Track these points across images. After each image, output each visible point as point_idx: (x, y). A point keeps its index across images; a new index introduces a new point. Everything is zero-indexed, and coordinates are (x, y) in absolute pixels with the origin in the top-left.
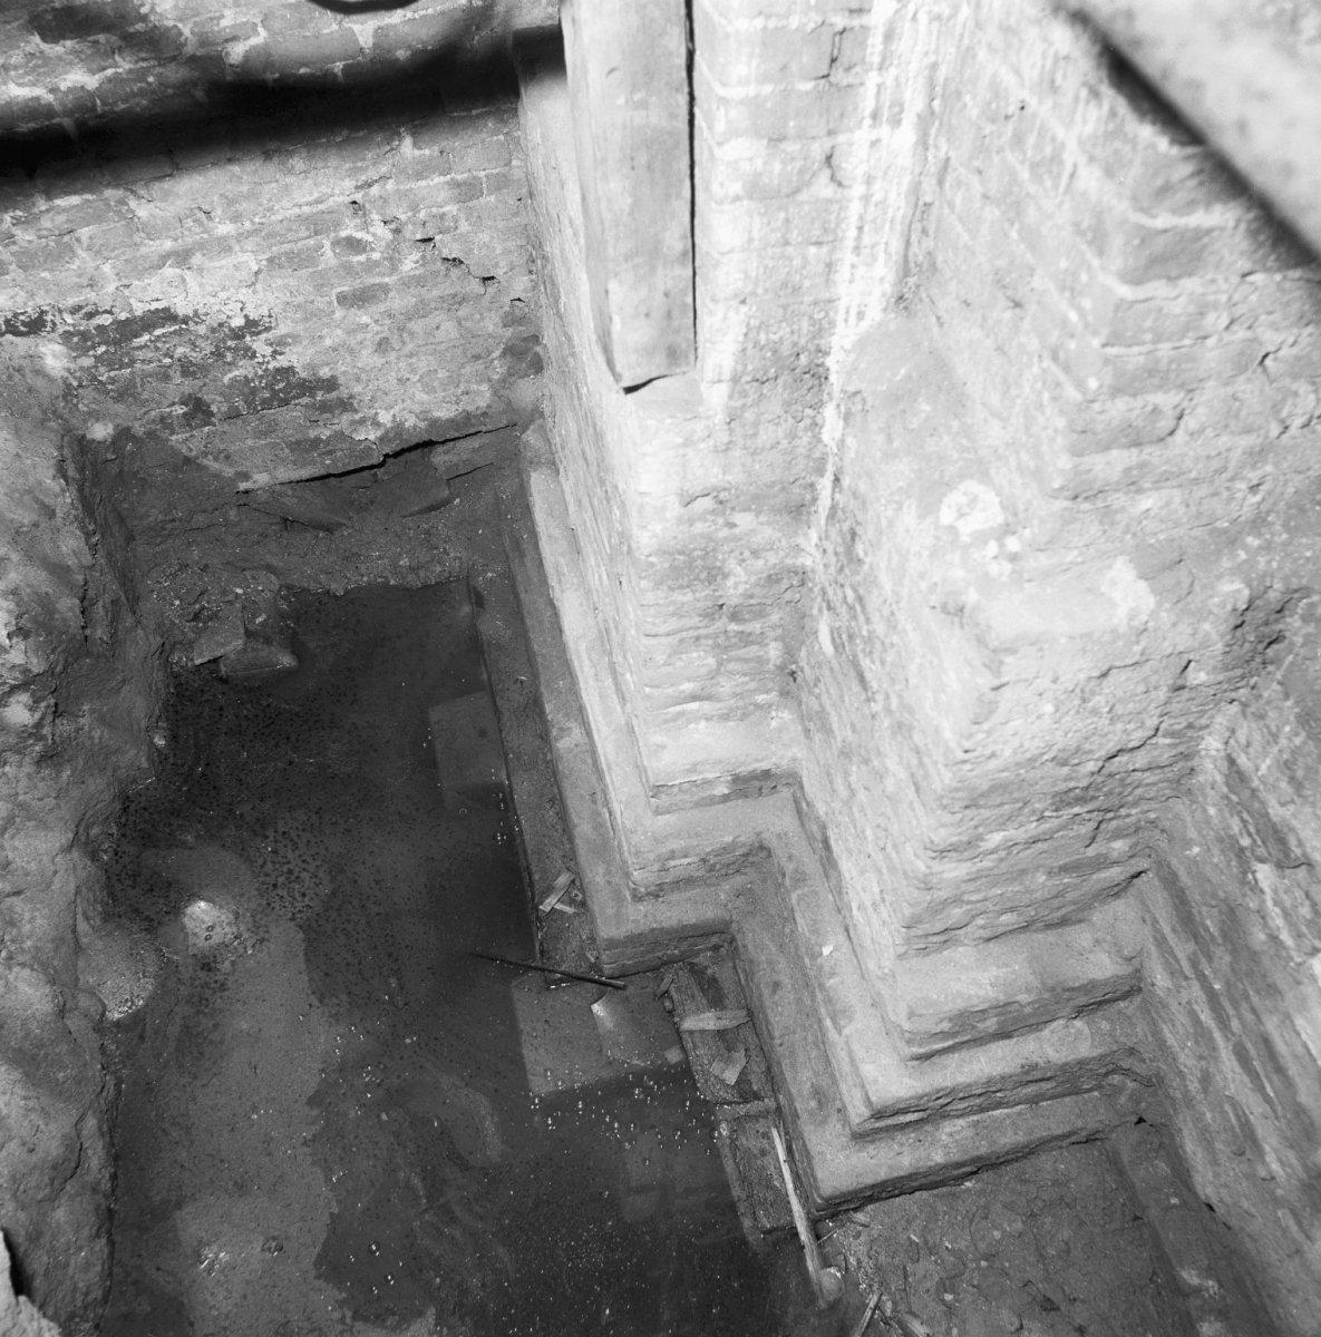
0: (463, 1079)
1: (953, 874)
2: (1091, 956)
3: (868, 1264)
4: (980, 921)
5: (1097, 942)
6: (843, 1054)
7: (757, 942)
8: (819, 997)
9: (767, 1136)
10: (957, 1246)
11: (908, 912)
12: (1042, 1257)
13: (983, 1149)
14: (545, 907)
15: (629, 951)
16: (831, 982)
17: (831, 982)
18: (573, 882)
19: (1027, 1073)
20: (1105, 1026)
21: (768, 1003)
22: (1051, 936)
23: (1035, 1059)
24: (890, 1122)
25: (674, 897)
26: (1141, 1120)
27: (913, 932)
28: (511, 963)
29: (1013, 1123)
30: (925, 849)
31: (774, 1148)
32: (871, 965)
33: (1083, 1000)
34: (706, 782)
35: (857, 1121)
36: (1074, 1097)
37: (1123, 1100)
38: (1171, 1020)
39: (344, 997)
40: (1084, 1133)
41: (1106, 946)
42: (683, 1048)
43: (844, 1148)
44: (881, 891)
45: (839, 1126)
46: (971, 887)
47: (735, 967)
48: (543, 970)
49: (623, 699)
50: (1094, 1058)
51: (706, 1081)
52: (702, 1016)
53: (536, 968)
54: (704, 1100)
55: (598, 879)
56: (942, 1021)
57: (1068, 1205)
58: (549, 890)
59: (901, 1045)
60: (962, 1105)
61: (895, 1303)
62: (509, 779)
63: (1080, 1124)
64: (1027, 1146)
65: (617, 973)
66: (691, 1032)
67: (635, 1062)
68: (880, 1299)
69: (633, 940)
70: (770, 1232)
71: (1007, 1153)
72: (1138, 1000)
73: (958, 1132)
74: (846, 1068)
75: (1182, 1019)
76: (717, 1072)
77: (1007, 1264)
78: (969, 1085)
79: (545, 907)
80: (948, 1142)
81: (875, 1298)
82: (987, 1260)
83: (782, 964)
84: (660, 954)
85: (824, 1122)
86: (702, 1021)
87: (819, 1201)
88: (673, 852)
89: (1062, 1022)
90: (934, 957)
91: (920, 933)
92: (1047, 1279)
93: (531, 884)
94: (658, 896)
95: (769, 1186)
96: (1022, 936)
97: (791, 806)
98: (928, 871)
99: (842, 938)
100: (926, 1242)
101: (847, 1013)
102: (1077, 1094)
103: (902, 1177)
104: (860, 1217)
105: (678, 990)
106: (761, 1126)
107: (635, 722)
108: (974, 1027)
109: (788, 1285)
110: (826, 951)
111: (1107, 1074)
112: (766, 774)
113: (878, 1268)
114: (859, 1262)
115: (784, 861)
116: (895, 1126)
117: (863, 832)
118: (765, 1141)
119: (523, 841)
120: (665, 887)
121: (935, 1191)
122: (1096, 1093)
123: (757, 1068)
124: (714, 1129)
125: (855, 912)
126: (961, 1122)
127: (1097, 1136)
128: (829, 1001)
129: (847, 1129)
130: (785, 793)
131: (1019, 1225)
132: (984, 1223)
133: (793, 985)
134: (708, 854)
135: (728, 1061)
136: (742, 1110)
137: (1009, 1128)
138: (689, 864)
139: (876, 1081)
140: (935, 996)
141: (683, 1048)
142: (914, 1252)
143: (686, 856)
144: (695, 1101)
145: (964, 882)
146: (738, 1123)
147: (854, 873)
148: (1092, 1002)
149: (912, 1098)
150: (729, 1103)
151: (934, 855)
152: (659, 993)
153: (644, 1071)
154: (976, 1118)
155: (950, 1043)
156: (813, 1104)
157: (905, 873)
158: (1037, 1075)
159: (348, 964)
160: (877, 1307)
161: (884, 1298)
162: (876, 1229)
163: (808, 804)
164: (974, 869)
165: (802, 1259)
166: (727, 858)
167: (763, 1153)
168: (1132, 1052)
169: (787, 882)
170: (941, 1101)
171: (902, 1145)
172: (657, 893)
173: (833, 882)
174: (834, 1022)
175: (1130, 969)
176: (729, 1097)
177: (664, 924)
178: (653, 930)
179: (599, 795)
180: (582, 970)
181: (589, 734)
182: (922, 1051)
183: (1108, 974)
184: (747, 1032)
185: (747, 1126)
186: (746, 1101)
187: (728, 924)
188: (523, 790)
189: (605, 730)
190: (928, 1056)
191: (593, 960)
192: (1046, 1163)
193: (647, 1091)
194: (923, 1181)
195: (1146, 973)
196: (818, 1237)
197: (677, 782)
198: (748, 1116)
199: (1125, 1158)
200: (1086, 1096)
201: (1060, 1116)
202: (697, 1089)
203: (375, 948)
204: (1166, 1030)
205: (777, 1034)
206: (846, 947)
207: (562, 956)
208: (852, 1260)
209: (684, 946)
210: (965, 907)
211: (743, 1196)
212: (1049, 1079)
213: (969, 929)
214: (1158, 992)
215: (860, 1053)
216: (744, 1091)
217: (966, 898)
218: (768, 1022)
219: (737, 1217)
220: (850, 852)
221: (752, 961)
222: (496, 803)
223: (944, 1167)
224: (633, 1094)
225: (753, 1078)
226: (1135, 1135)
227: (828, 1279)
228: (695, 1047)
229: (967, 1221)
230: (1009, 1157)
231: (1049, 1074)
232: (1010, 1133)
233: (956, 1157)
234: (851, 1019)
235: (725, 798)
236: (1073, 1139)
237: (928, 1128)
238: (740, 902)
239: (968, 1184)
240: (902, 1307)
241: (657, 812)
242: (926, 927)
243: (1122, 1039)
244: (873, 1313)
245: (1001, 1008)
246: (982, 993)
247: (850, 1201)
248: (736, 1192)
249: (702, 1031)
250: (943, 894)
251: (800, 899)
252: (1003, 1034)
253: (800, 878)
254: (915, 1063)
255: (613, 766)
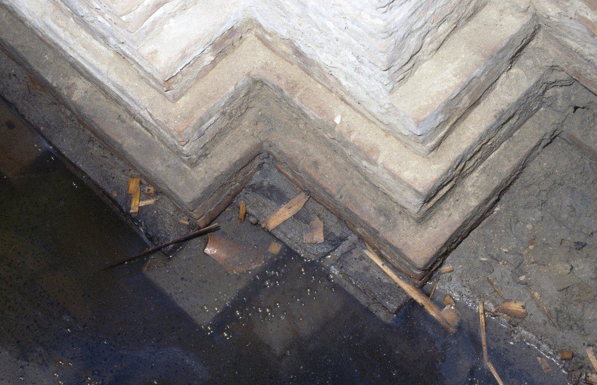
0: (153, 346)
1: (401, 16)
2: (502, 22)
3: (466, 291)
4: (428, 40)
5: (502, 11)
6: (386, 176)
7: (288, 144)
8: (349, 152)
9: (363, 258)
10: (510, 248)
11: (384, 58)
12: (561, 223)
13: (496, 181)
14: (134, 209)
15: (209, 201)
16: (353, 137)
17: (353, 137)
18: (141, 183)
19: (500, 119)
20: (529, 62)
21: (317, 177)
22: (472, 24)
23: (500, 107)
24: (435, 199)
25: (218, 148)
26: (576, 108)
27: (393, 70)
28: (135, 258)
29: (505, 156)
30: (377, 9)
31: (372, 261)
32: (375, 109)
33: (511, 53)
34: (196, 59)
35: (416, 210)
36: (531, 119)
37: (560, 102)
38: (570, 32)
39: (40, 349)
40: (547, 137)
41: (508, 11)
42: (278, 240)
43: (416, 233)
44: (358, 57)
45: (405, 222)
46: (414, 18)
47: (279, 171)
48: (159, 249)
49: (104, 39)
50: (533, 86)
51: (305, 250)
52: (278, 213)
53: (154, 251)
54: (311, 261)
55: (159, 169)
56: (437, 116)
57: (560, 184)
58: (129, 198)
59: (418, 147)
60: (471, 163)
61: (493, 302)
62: (50, 143)
63: (542, 132)
64: (520, 165)
65: (208, 221)
66: (277, 228)
67: (254, 267)
68: (483, 305)
69: (208, 192)
70: (398, 311)
71: (511, 176)
72: (541, 34)
73: (477, 181)
74: (392, 183)
75: (576, 26)
76: (309, 241)
77: (544, 239)
78: (471, 147)
79: (134, 209)
80: (474, 191)
81: (481, 306)
82: (532, 244)
83: (312, 149)
84: (228, 192)
85: (395, 226)
86: (279, 217)
87: (418, 273)
88: (201, 119)
89: (504, 75)
90: (411, 80)
91: (396, 68)
92: (571, 232)
93: (115, 202)
94: (206, 155)
95: (381, 284)
96: (456, 35)
97: (258, 43)
98: (385, 23)
99: (343, 107)
100: (492, 257)
101: (375, 150)
102: (531, 116)
103: (459, 228)
104: (446, 268)
105: (253, 207)
106: (355, 254)
107: (124, 48)
108: (457, 109)
109: (427, 332)
110: (337, 120)
111: (544, 92)
112: (232, 31)
113: (473, 290)
114: (460, 293)
115: (275, 82)
116: (438, 200)
117: (325, 26)
118: (364, 261)
119: (89, 178)
120: (207, 146)
121: (480, 226)
122: (542, 109)
123: (332, 221)
124: (328, 275)
125: (344, 83)
126: (475, 174)
127: (556, 134)
128: (358, 150)
129: (412, 221)
130: (250, 37)
131: (539, 213)
132: (518, 225)
133: (326, 157)
134: (224, 107)
135: (312, 230)
136: (338, 253)
137: (503, 161)
138: (215, 121)
139: (416, 179)
140: (426, 103)
141: (278, 240)
142: (488, 267)
143: (210, 117)
144: (308, 266)
145: (409, 17)
146: (341, 262)
147: (331, 58)
148: (517, 51)
149: (442, 176)
150: (328, 254)
151: (384, 9)
152: (242, 216)
153: (265, 268)
154: (481, 167)
155: (448, 127)
156: (382, 219)
157: (371, 34)
158: (507, 116)
159: (28, 327)
160: (485, 311)
161: (486, 303)
162: (459, 268)
163: (270, 35)
164: (412, 6)
165: (426, 315)
166: (237, 103)
167: (367, 269)
168: (553, 68)
169: (286, 93)
170: (460, 167)
171: (448, 209)
172: (204, 153)
173: (316, 75)
174: (368, 160)
175: (530, 17)
176: (326, 250)
177: (221, 170)
178: (216, 178)
179: (124, 116)
180: (184, 233)
181: (89, 78)
182: (434, 143)
183: (519, 27)
184: (313, 205)
185: (347, 260)
186: (337, 246)
187: (260, 145)
188: (67, 146)
189: (104, 68)
190: (439, 144)
191: (187, 223)
192: (534, 167)
193: (273, 278)
194: (472, 222)
195: (540, 12)
196: (428, 295)
197: (178, 70)
198: (344, 254)
199: (578, 136)
200: (537, 114)
201: (529, 134)
202: (303, 258)
203: (39, 305)
204: (568, 41)
205: (334, 192)
206: (348, 110)
207: (165, 233)
208: (455, 295)
209: (241, 177)
210: (417, 35)
211: (371, 301)
212: (514, 115)
213: (423, 49)
214: (554, 19)
215: (395, 168)
216: (334, 241)
217: (414, 28)
218: (324, 189)
219: (374, 316)
220: (321, 46)
221: (291, 159)
222: (55, 165)
223: (480, 207)
224: (266, 286)
225: (333, 230)
226: (578, 117)
227: (447, 315)
228: (285, 235)
229: (508, 230)
230: (513, 177)
231: (512, 112)
232: (506, 162)
233: (483, 196)
234: (378, 152)
235: (214, 63)
236: (543, 144)
237: (458, 189)
238: (260, 126)
239: (497, 209)
240: (499, 301)
241: (175, 99)
242: (400, 62)
243: (545, 64)
244: (485, 315)
245: (466, 87)
246: (452, 84)
247: (437, 262)
248: (362, 299)
249: (284, 222)
250: (401, 33)
251: (301, 100)
252: (475, 104)
253: (294, 86)
254: (432, 153)
255: (125, 88)
